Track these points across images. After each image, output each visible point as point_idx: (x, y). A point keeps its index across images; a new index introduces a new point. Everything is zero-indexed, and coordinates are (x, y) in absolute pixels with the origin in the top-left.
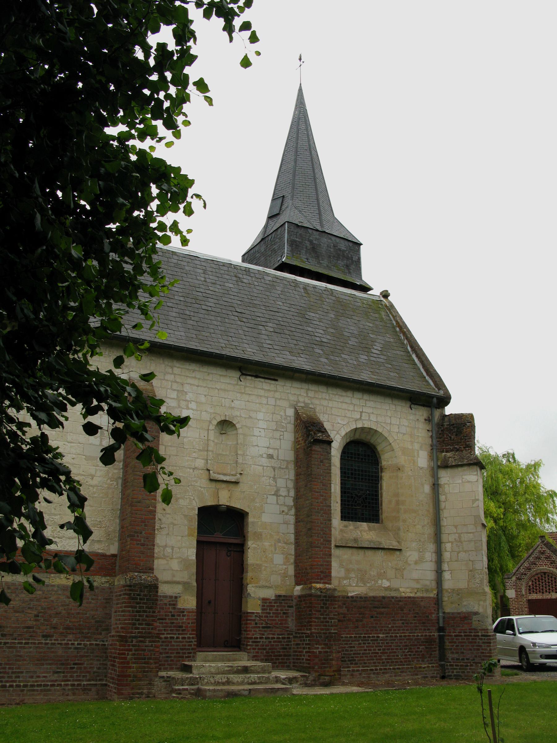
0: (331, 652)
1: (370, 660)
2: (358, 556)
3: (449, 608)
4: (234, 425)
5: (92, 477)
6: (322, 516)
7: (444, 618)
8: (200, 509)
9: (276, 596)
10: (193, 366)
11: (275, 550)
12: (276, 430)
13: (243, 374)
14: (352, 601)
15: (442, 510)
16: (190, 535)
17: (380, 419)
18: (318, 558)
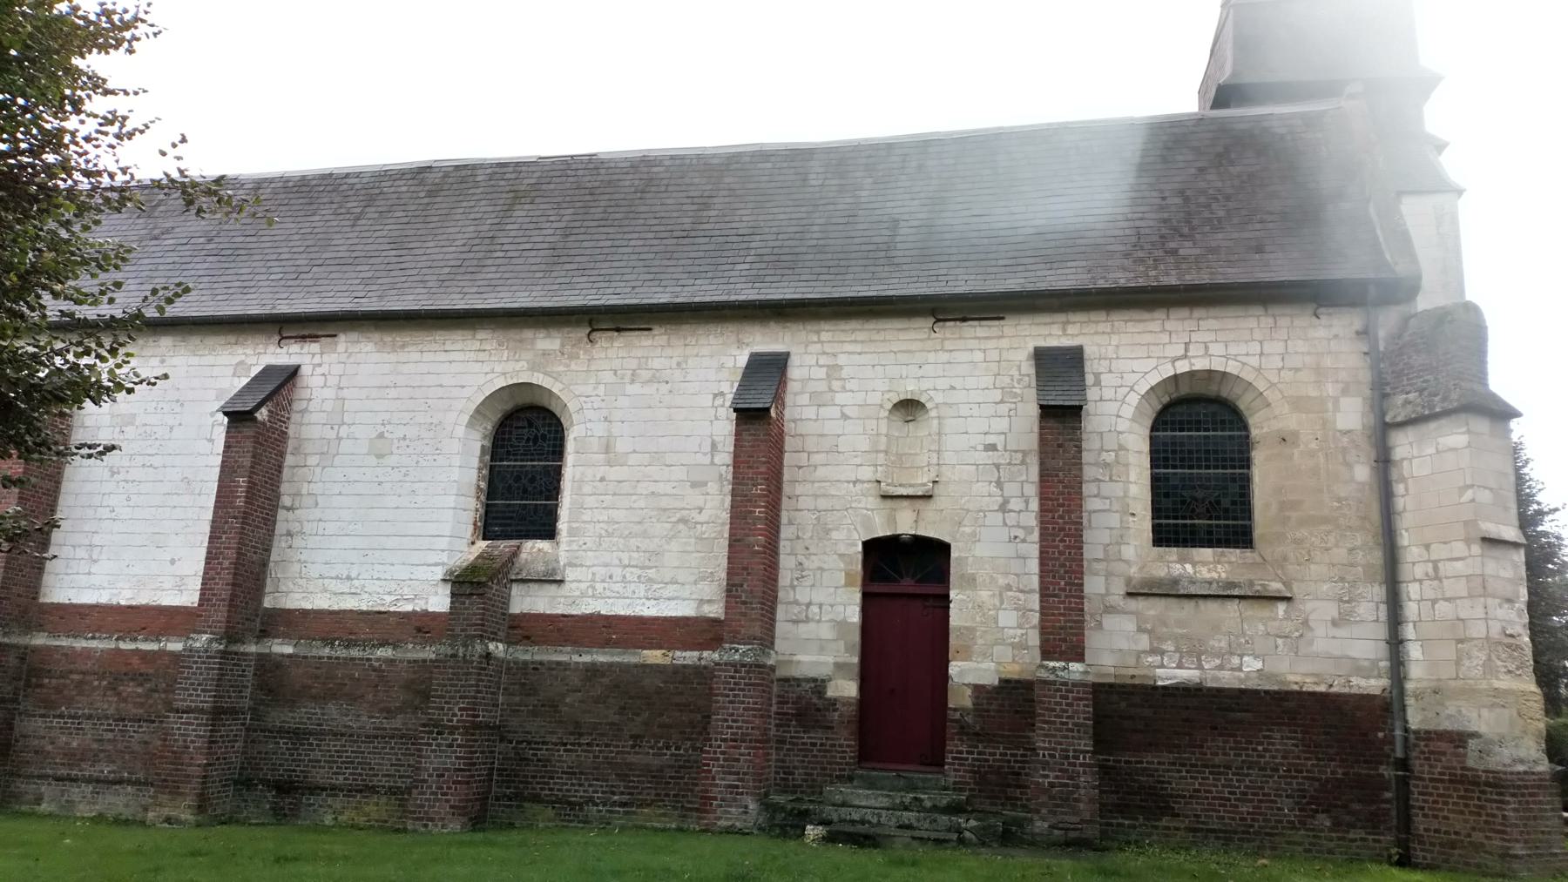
0: (1077, 787)
1: (1208, 811)
2: (1179, 611)
3: (1415, 720)
4: (923, 406)
5: (701, 510)
6: (1062, 541)
7: (1406, 739)
8: (865, 544)
9: (1001, 680)
10: (853, 324)
11: (1002, 603)
12: (1002, 402)
13: (939, 320)
14: (1163, 695)
15: (1399, 514)
16: (848, 584)
17: (1233, 350)
18: (1053, 615)
